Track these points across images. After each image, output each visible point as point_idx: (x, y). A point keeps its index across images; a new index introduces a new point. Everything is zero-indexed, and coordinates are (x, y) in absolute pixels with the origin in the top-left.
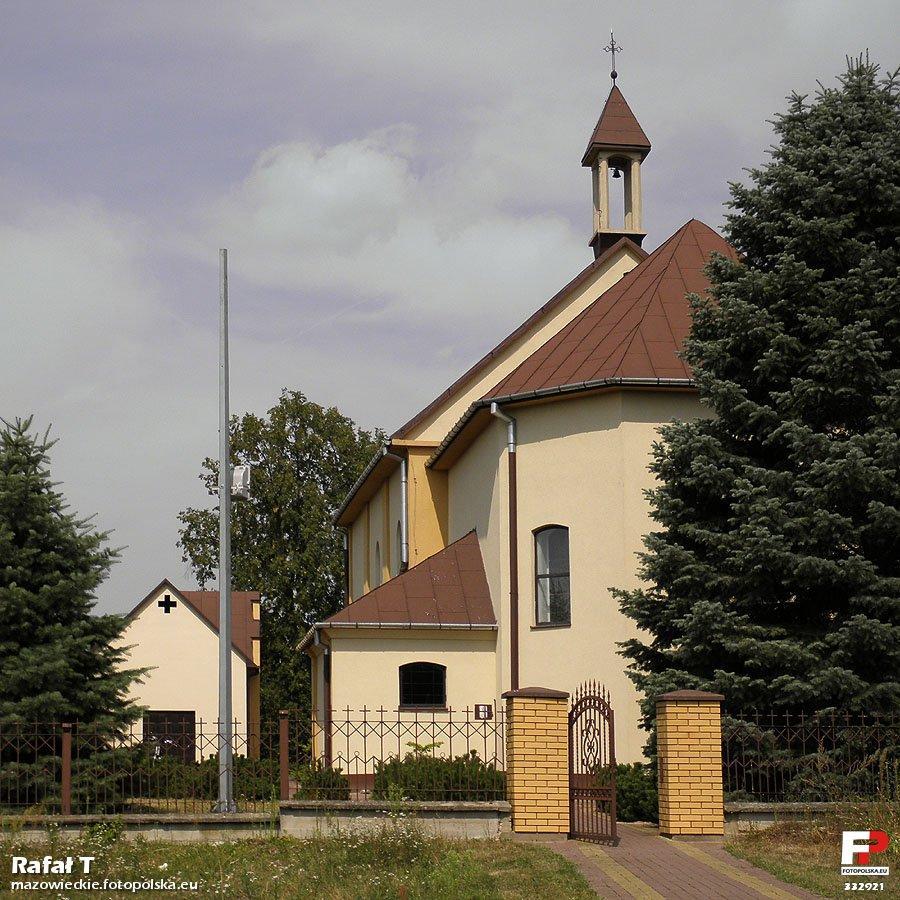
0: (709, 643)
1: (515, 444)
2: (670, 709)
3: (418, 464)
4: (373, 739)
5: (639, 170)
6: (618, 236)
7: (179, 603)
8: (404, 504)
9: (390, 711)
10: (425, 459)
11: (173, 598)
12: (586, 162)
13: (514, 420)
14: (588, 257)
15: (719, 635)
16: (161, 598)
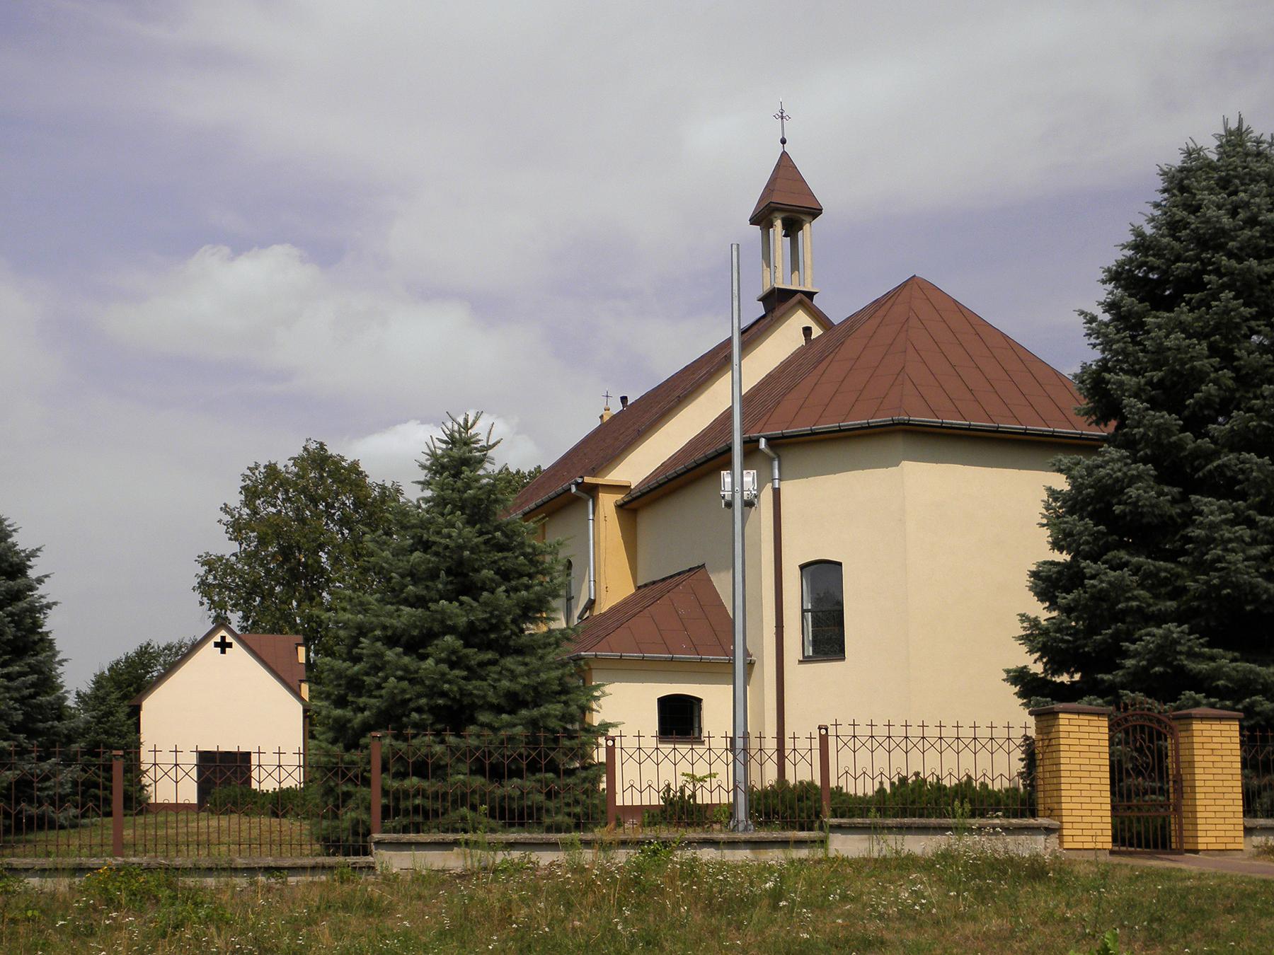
0: (1169, 664)
1: (780, 480)
2: (1197, 726)
3: (607, 502)
4: (881, 754)
5: (811, 231)
6: (795, 292)
7: (235, 644)
8: (591, 542)
9: (914, 726)
10: (619, 497)
11: (229, 639)
12: (754, 221)
13: (779, 457)
14: (760, 310)
15: (1182, 657)
16: (217, 639)
